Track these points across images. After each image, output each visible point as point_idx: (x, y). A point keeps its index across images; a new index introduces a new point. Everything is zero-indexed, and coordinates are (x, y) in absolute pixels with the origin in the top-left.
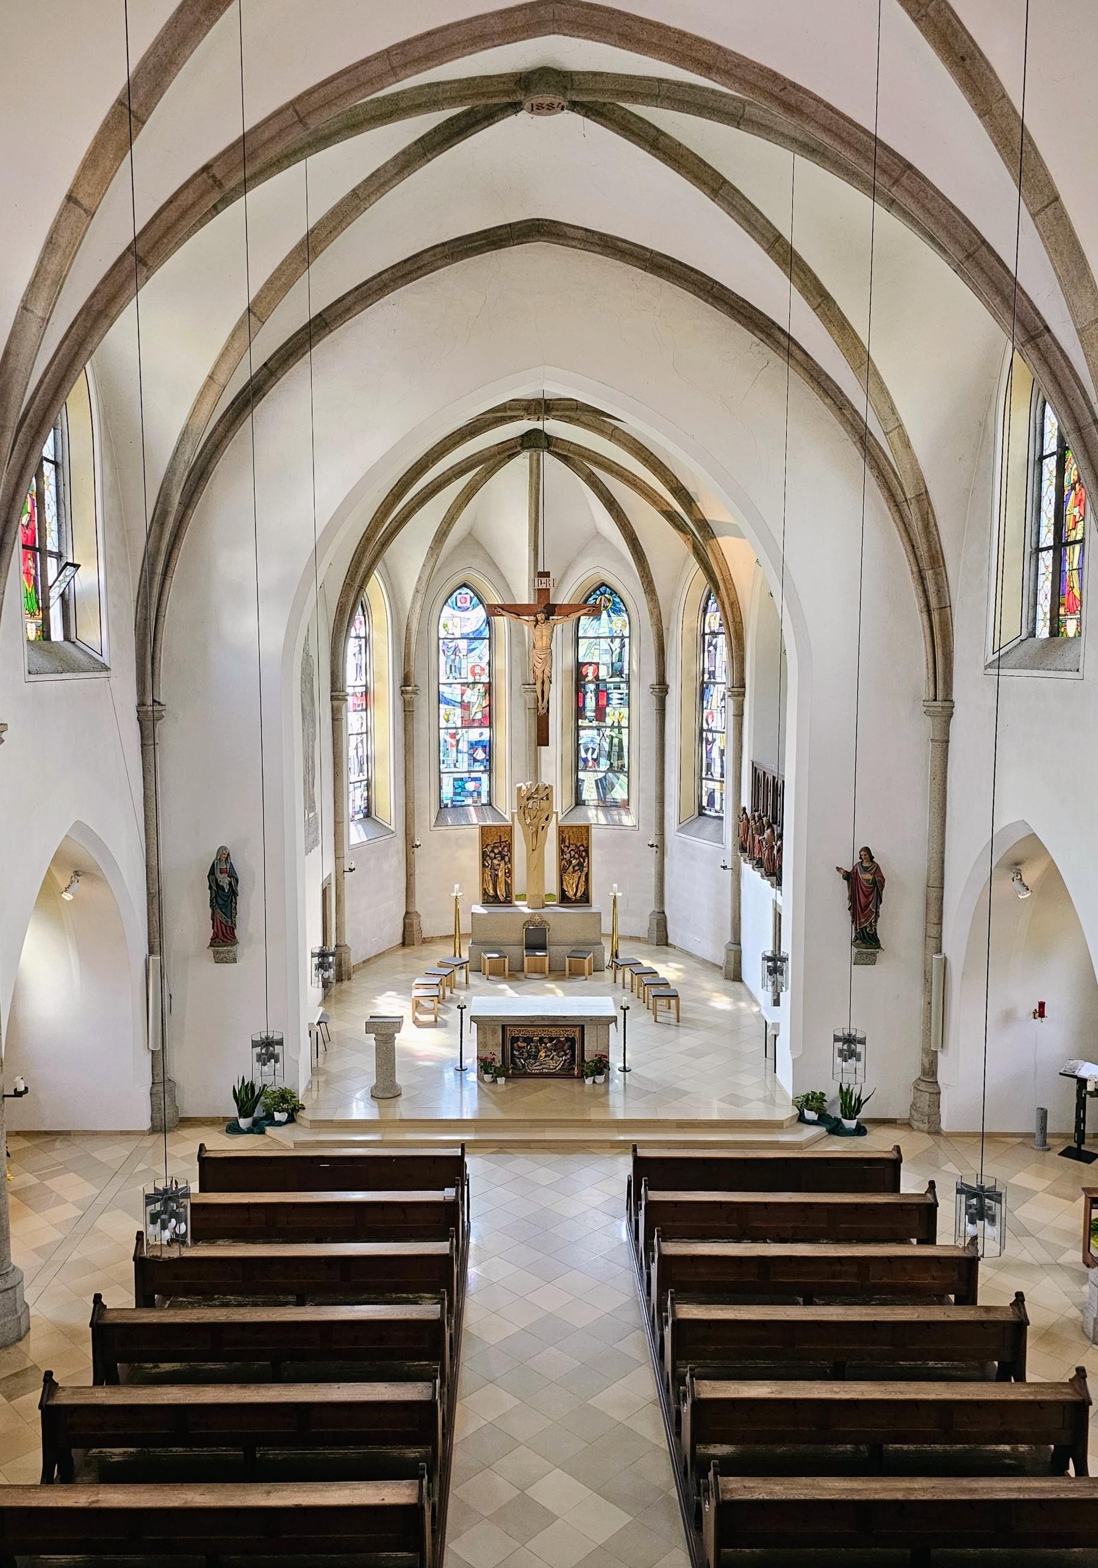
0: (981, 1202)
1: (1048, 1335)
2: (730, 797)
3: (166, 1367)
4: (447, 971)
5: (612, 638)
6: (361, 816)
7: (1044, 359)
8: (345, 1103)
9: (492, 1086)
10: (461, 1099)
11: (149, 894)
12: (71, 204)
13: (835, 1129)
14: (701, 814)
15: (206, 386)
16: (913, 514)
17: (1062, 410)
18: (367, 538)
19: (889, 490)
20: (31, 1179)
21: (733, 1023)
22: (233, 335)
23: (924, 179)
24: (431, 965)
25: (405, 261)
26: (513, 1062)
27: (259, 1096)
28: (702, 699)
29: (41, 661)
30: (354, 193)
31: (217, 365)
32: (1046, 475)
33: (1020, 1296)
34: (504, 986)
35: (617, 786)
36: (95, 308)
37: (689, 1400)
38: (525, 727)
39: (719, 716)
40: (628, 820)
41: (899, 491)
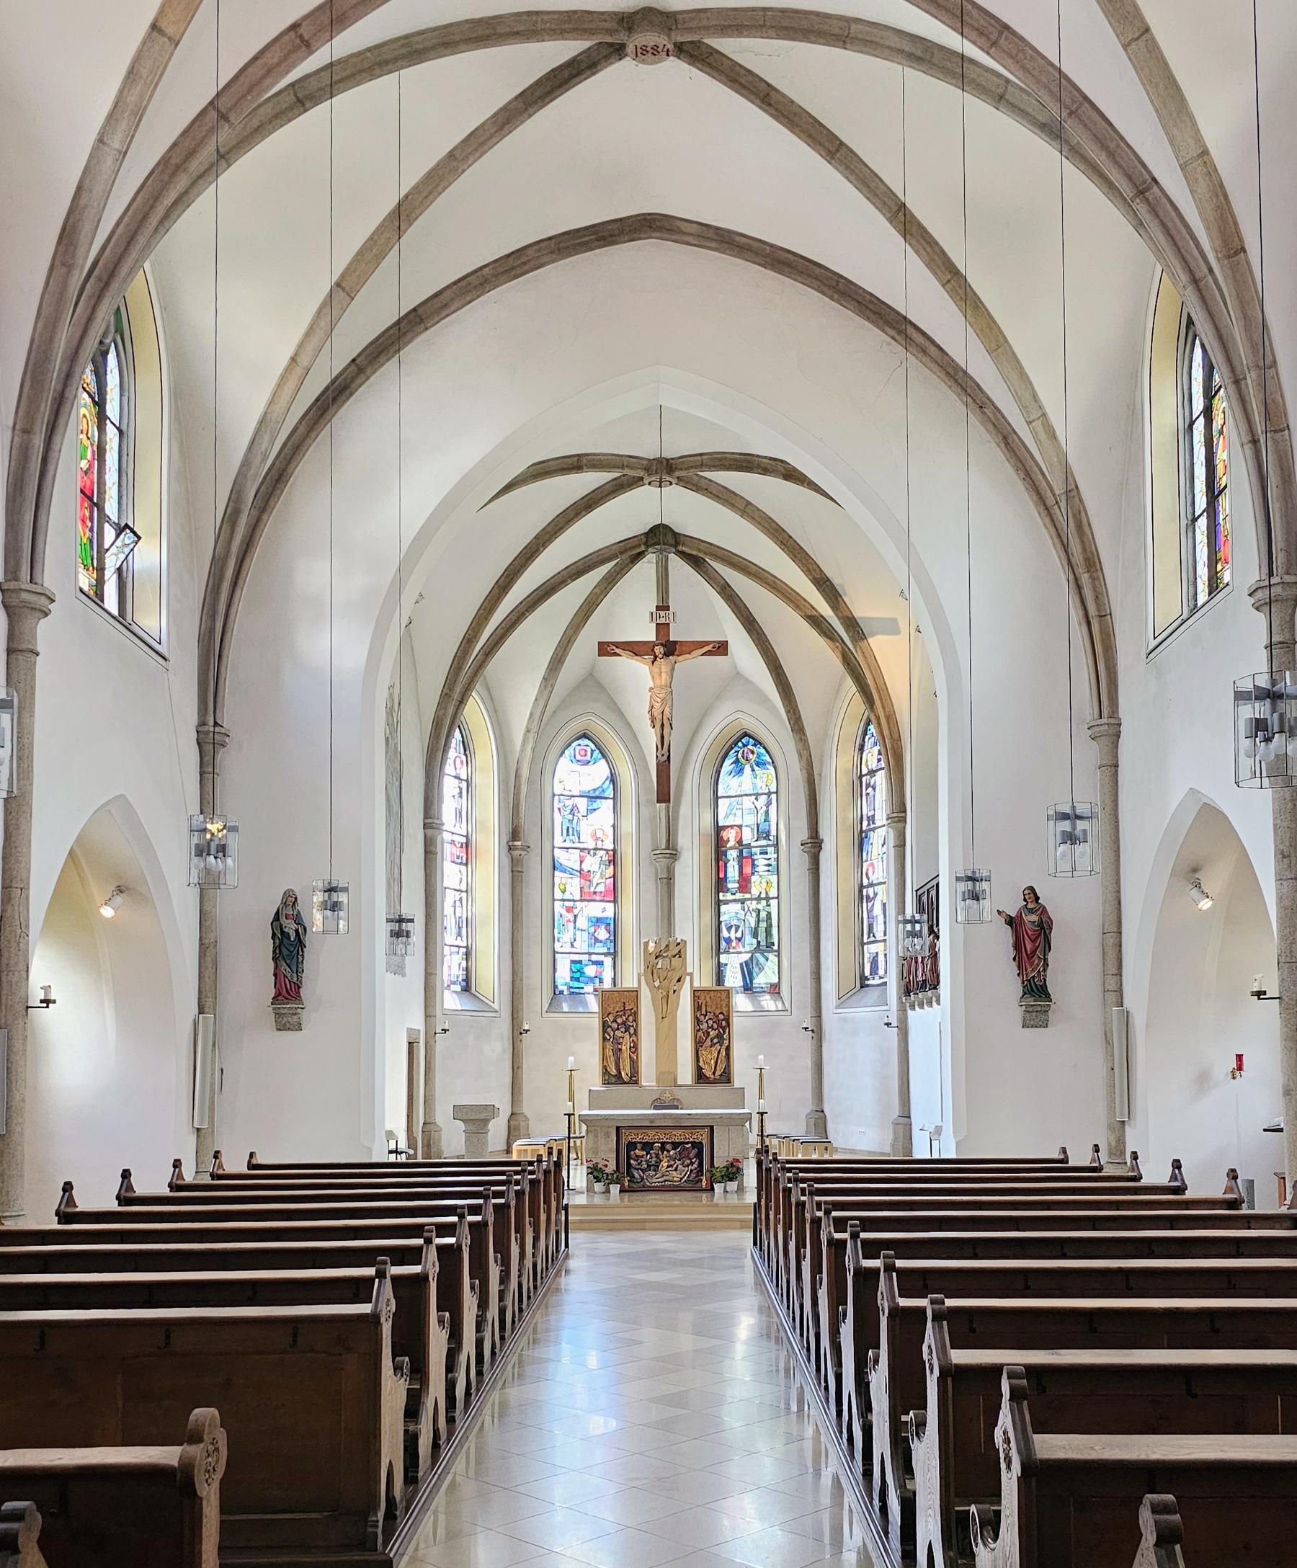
5: (757, 795)
6: (458, 988)
12: (155, 33)
16: (1062, 513)
23: (1021, 38)
25: (508, 256)
26: (630, 1174)
28: (861, 850)
30: (451, 155)
31: (301, 345)
36: (173, 161)
41: (1049, 493)
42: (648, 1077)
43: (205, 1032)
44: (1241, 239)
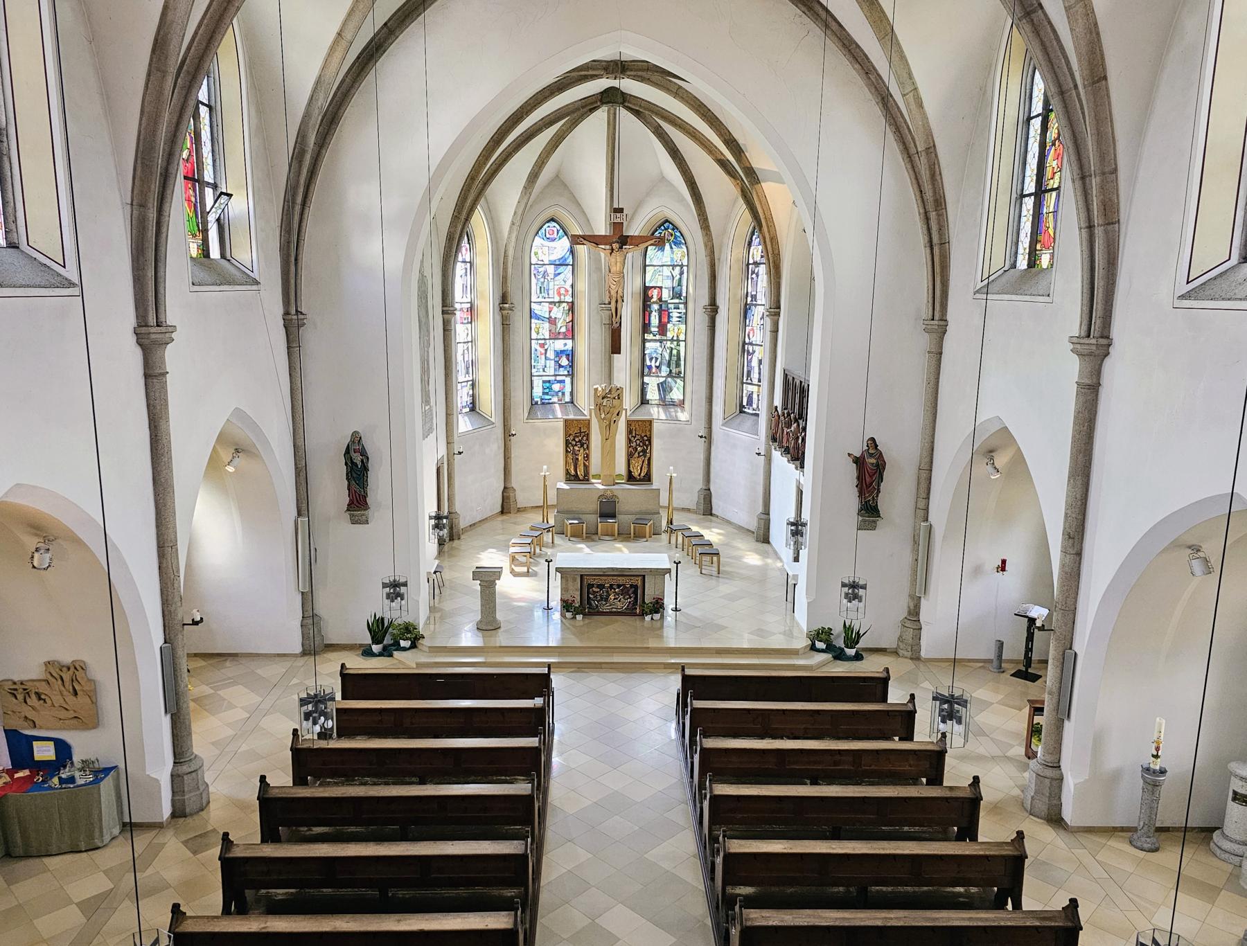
0: (951, 708)
1: (996, 808)
2: (766, 397)
3: (318, 830)
4: (537, 533)
5: (674, 266)
7: (1036, 31)
8: (456, 634)
9: (572, 622)
10: (548, 631)
11: (296, 468)
13: (839, 656)
14: (741, 412)
17: (1048, 76)
18: (472, 178)
19: (904, 143)
20: (206, 690)
21: (761, 576)
24: (525, 529)
27: (388, 627)
28: (745, 318)
29: (202, 275)
32: (1032, 133)
33: (976, 780)
34: (582, 546)
35: (675, 389)
37: (722, 854)
38: (601, 339)
39: (758, 332)
40: (683, 416)
41: (912, 145)
43: (303, 532)
44: (1104, 69)
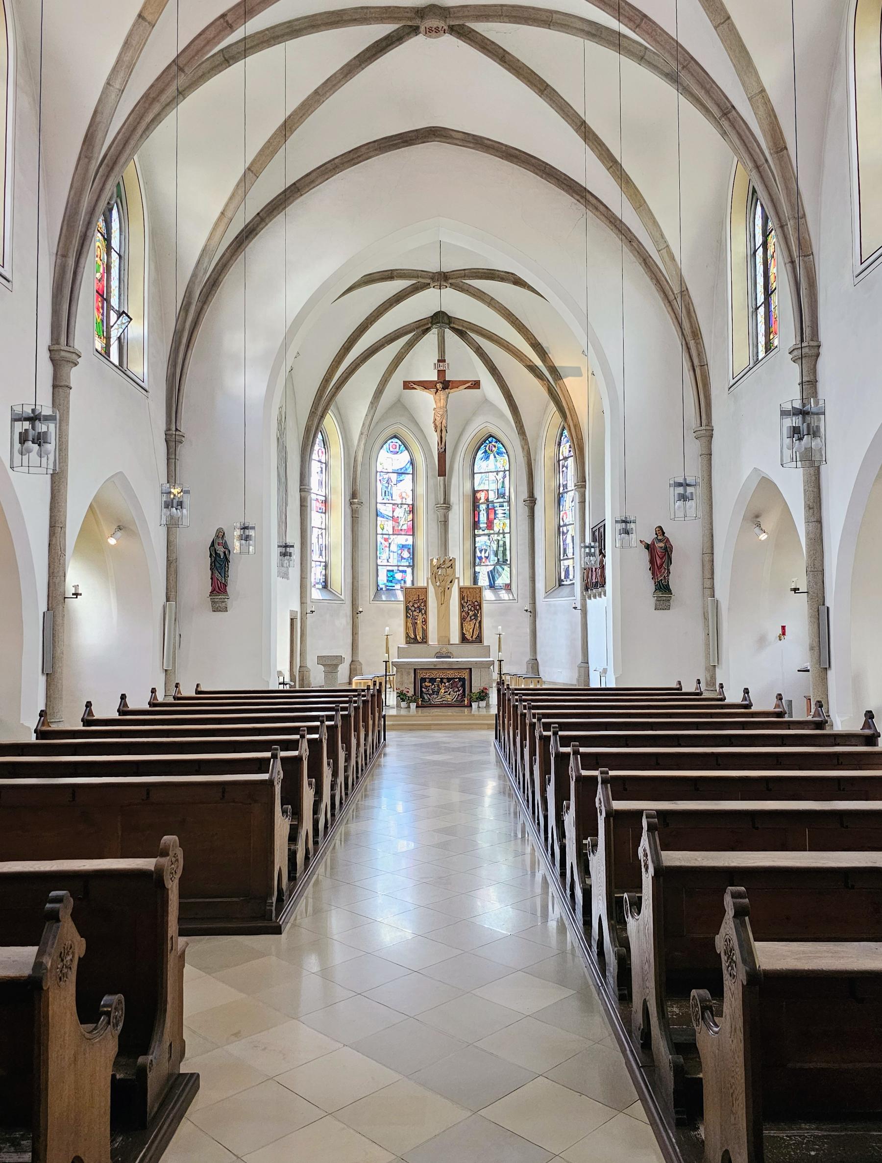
5: (497, 472)
6: (320, 587)
15: (220, 219)
16: (678, 304)
19: (664, 293)
22: (237, 185)
23: (654, 23)
25: (350, 152)
26: (422, 697)
30: (316, 92)
31: (227, 205)
36: (152, 96)
41: (671, 293)
42: (433, 639)
44: (784, 142)
